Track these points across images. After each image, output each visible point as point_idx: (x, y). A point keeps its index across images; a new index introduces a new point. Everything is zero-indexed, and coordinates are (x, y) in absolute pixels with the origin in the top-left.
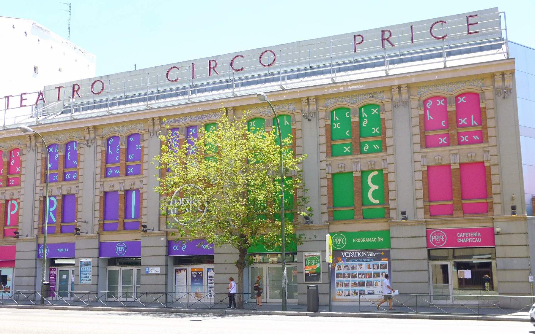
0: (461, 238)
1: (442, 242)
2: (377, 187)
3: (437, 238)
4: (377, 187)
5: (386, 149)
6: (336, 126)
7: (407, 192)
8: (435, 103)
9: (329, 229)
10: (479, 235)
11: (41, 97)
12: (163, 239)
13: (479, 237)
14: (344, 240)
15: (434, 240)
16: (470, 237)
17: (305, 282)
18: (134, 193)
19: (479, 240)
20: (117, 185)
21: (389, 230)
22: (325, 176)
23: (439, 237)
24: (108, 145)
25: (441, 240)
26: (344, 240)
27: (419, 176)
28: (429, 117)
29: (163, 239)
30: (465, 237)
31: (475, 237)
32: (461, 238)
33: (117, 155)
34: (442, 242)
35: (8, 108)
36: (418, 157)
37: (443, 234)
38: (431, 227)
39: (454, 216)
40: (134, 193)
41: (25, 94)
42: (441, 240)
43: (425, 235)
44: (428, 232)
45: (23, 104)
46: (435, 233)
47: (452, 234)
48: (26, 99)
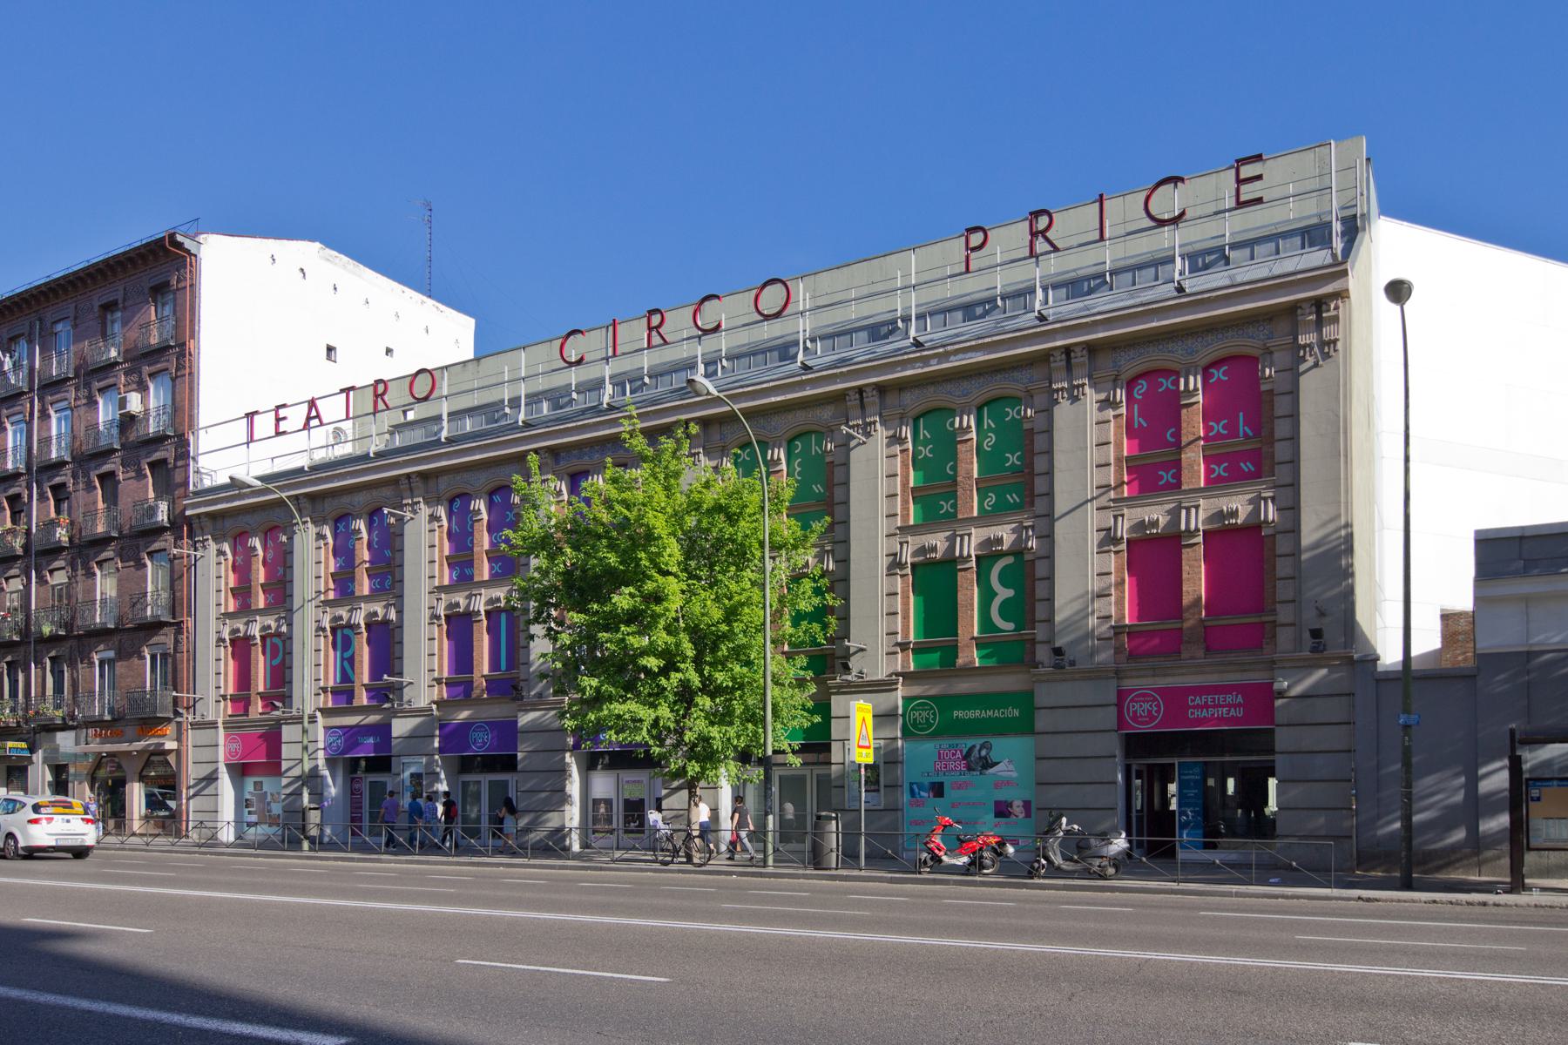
0: (1197, 707)
1: (1152, 718)
2: (1010, 593)
4: (1010, 593)
8: (1154, 386)
10: (1240, 699)
11: (314, 413)
13: (1239, 705)
14: (1158, 706)
15: (1135, 712)
16: (1219, 706)
18: (503, 617)
19: (1239, 713)
23: (1146, 706)
25: (1150, 712)
30: (1206, 706)
31: (1229, 706)
32: (1197, 707)
34: (1152, 718)
38: (1128, 684)
39: (1184, 655)
40: (503, 617)
41: (284, 406)
42: (1150, 712)
43: (1115, 700)
44: (1122, 695)
45: (1242, 176)
47: (1175, 698)
48: (1259, 177)
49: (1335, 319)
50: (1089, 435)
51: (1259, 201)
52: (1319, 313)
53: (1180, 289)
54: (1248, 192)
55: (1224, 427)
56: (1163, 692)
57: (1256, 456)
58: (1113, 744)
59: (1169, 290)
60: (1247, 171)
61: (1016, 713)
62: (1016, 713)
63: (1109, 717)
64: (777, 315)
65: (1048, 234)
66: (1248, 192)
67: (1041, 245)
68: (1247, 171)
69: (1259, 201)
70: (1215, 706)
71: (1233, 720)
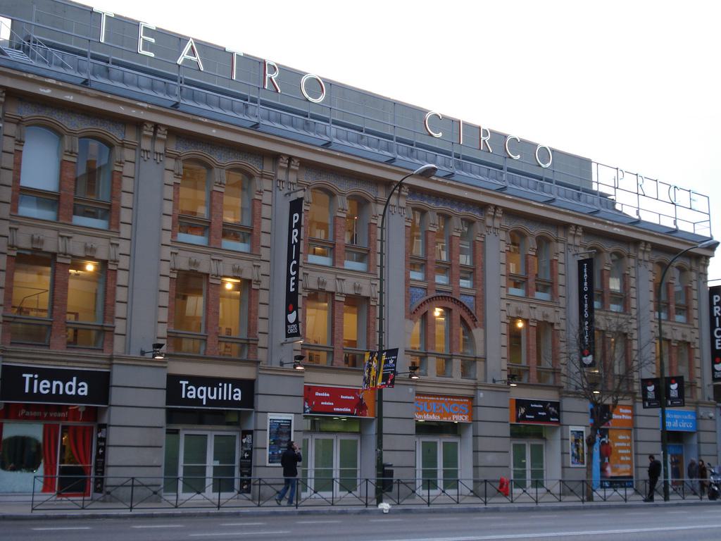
5: (118, 227)
12: (481, 394)
17: (268, 464)
27: (165, 284)
29: (481, 394)
52: (155, 133)
63: (161, 398)
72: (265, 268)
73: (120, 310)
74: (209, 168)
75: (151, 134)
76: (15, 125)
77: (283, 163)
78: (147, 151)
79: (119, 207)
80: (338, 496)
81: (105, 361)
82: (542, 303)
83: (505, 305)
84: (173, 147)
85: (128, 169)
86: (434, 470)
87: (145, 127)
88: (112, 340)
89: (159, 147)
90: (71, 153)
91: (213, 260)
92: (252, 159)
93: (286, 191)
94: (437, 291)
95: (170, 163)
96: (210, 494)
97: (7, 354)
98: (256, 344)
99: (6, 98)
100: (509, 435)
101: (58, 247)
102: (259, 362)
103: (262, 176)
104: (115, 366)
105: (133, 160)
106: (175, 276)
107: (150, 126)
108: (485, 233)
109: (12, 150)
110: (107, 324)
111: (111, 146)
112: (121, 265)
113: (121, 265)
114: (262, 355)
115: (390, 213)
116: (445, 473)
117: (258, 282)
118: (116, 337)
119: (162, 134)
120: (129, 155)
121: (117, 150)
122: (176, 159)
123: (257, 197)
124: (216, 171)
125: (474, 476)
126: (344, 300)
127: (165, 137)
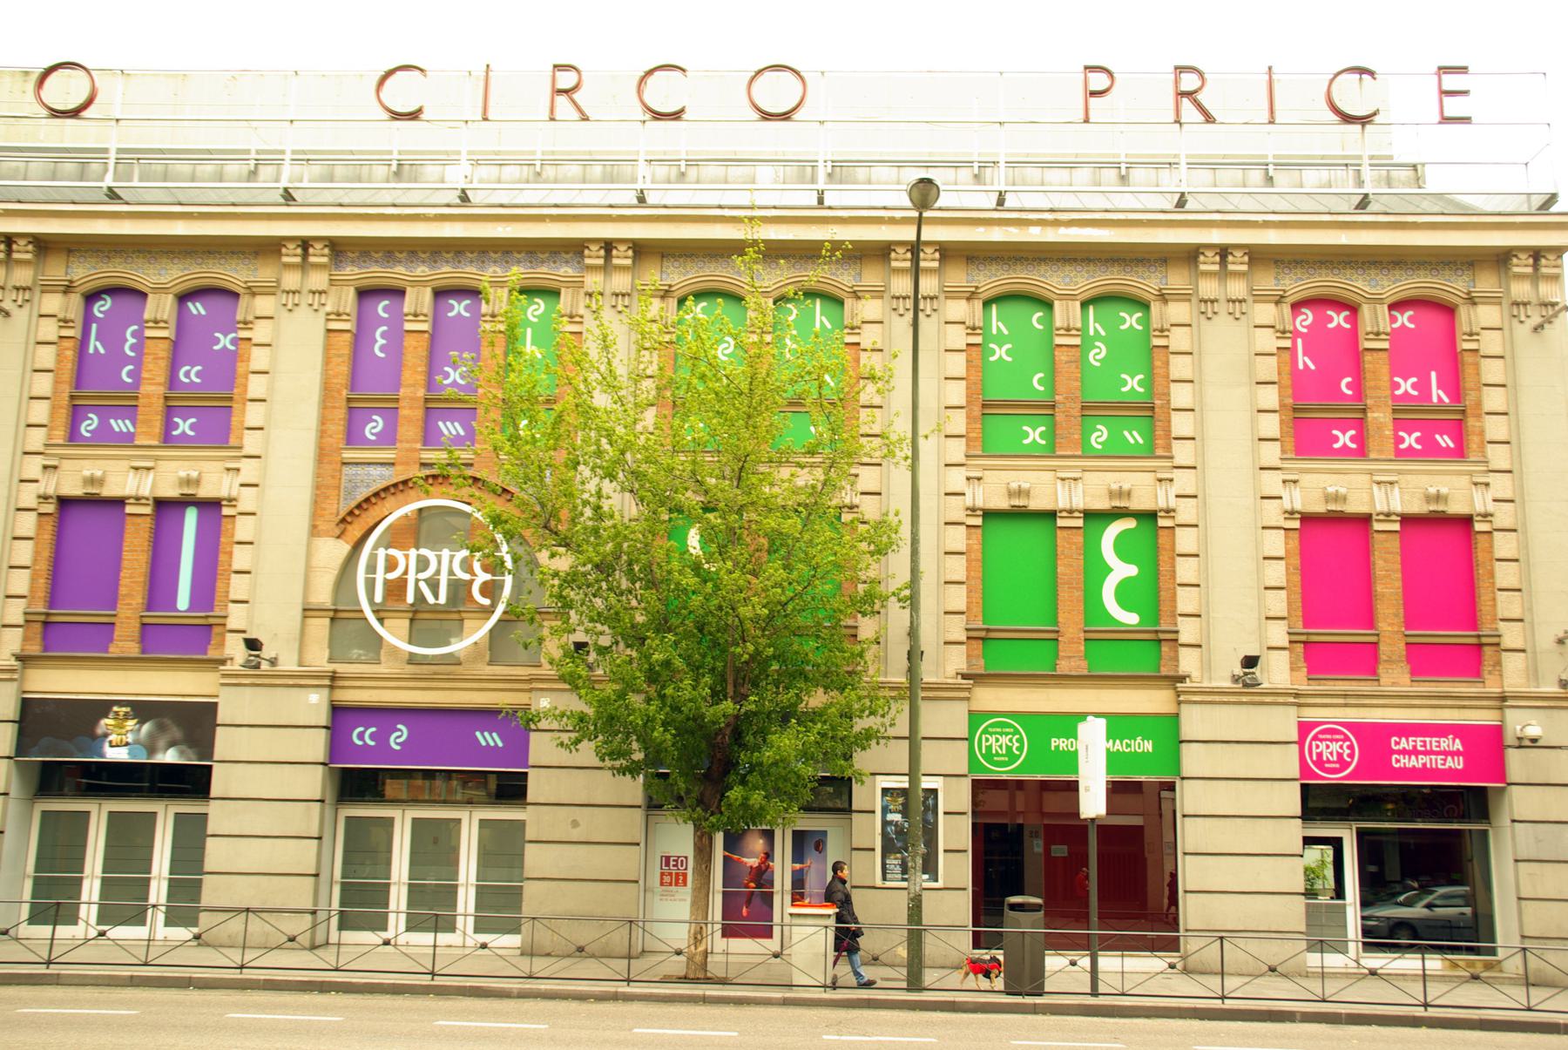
0: (1404, 752)
2: (1132, 570)
3: (999, 743)
4: (1132, 570)
5: (1168, 447)
6: (1000, 353)
7: (1239, 596)
9: (22, 680)
10: (1458, 745)
13: (1457, 753)
16: (1432, 752)
17: (879, 883)
19: (1457, 764)
20: (1385, 489)
21: (1177, 715)
22: (959, 515)
23: (1335, 747)
24: (88, 318)
26: (1020, 741)
27: (1276, 543)
28: (95, 345)
31: (1446, 753)
32: (1404, 752)
33: (128, 361)
35: (1087, 121)
36: (33, 467)
37: (1347, 739)
38: (1311, 714)
41: (1463, 70)
43: (1295, 737)
46: (991, 725)
47: (1374, 739)
48: (1465, 93)
49: (1556, 278)
50: (1230, 367)
51: (1465, 120)
52: (305, 255)
53: (642, 200)
54: (1454, 107)
55: (1414, 386)
56: (1353, 727)
57: (1458, 429)
58: (313, 782)
59: (991, 202)
60: (1451, 82)
61: (1054, 742)
62: (1148, 746)
63: (316, 745)
64: (75, 113)
65: (1200, 97)
66: (1454, 107)
67: (1189, 110)
68: (1451, 82)
69: (1465, 120)
70: (1425, 753)
71: (1451, 773)
72: (1185, 482)
73: (1186, 601)
74: (1047, 305)
75: (1529, 270)
76: (964, 302)
77: (1209, 263)
78: (1525, 304)
79: (1169, 409)
80: (159, 936)
81: (347, 683)
82: (1115, 455)
83: (40, 468)
84: (1267, 281)
85: (1491, 343)
86: (1087, 916)
87: (1515, 260)
88: (1498, 663)
89: (1237, 288)
90: (1068, 330)
91: (136, 469)
92: (1130, 268)
93: (1536, 319)
94: (423, 465)
95: (53, 303)
96: (464, 934)
97: (1302, 701)
98: (1498, 644)
99: (1251, 263)
100: (1298, 812)
101: (1057, 501)
102: (1182, 679)
103: (1472, 301)
104: (1508, 712)
105: (1497, 324)
106: (1296, 524)
107: (1210, 253)
108: (582, 311)
109: (54, 338)
110: (1163, 628)
111: (1449, 310)
112: (1181, 518)
113: (1181, 518)
114: (1188, 662)
115: (1515, 321)
116: (173, 885)
117: (1486, 516)
118: (1183, 651)
119: (1238, 263)
120: (1178, 311)
121: (1155, 308)
122: (1277, 303)
123: (1157, 342)
124: (1366, 311)
125: (910, 921)
126: (1397, 527)
127: (1245, 268)
